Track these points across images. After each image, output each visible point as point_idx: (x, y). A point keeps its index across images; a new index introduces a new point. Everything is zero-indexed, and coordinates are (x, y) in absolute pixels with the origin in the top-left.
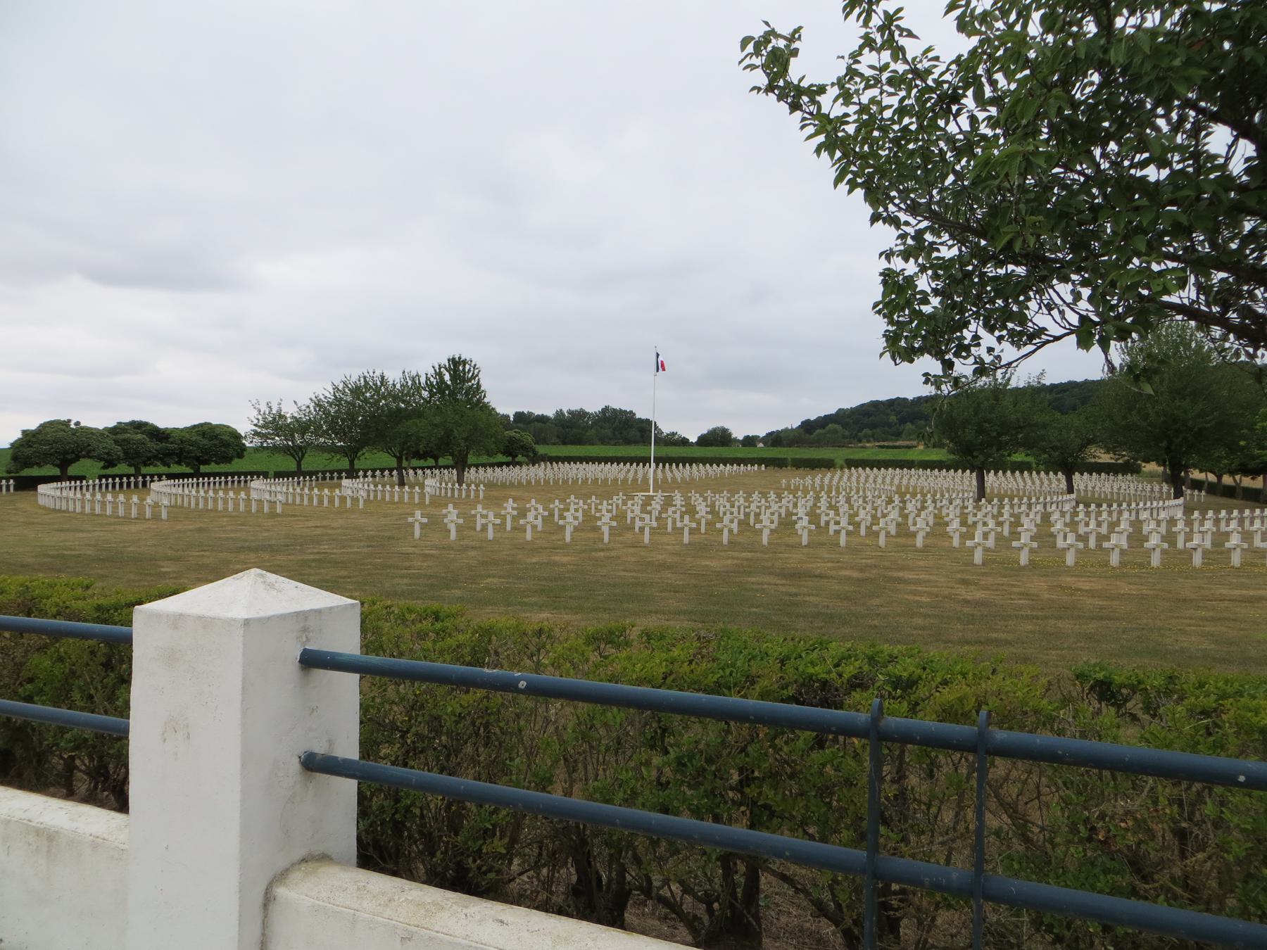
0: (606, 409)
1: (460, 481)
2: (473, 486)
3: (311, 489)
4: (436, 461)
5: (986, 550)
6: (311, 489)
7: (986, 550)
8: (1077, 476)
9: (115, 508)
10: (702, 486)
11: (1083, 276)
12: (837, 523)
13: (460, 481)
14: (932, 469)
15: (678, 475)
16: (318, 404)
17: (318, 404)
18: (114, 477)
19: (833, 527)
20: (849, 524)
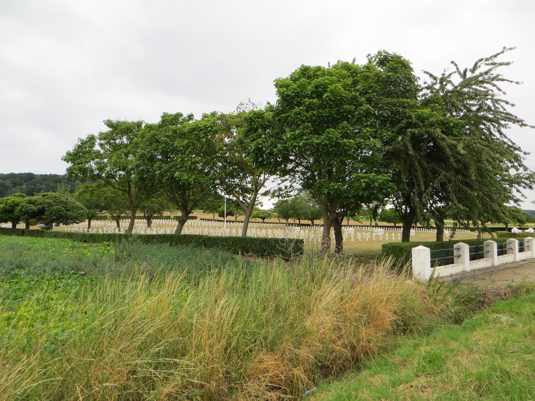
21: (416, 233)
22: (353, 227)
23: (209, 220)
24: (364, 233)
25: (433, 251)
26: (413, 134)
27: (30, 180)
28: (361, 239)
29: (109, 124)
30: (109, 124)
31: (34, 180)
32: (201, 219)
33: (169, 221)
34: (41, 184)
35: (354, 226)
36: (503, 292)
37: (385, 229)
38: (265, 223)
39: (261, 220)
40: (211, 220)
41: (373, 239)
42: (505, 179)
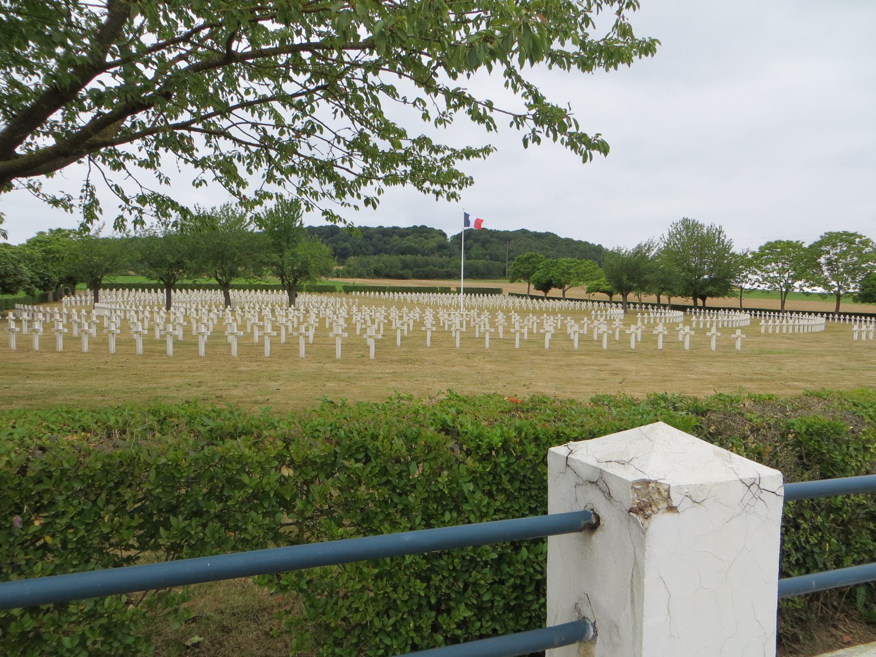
0: (600, 246)
1: (292, 302)
2: (148, 308)
3: (705, 317)
4: (625, 296)
5: (462, 332)
6: (705, 317)
7: (462, 332)
8: (101, 291)
9: (781, 328)
10: (553, 312)
11: (516, 51)
12: (261, 328)
13: (292, 302)
14: (239, 290)
15: (537, 307)
16: (822, 237)
17: (822, 237)
18: (593, 301)
19: (257, 333)
20: (273, 330)
21: (751, 323)
22: (825, 315)
23: (518, 296)
24: (545, 315)
25: (789, 484)
26: (101, 626)
27: (332, 236)
28: (528, 333)
29: (400, 77)
30: (400, 77)
31: (337, 236)
32: (511, 294)
33: (471, 298)
34: (345, 241)
35: (822, 314)
36: (318, 409)
37: (828, 318)
38: (566, 299)
39: (606, 297)
40: (523, 296)
41: (601, 346)
42: (144, 99)
